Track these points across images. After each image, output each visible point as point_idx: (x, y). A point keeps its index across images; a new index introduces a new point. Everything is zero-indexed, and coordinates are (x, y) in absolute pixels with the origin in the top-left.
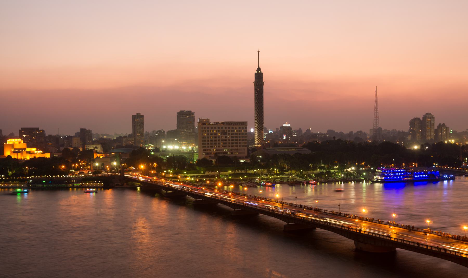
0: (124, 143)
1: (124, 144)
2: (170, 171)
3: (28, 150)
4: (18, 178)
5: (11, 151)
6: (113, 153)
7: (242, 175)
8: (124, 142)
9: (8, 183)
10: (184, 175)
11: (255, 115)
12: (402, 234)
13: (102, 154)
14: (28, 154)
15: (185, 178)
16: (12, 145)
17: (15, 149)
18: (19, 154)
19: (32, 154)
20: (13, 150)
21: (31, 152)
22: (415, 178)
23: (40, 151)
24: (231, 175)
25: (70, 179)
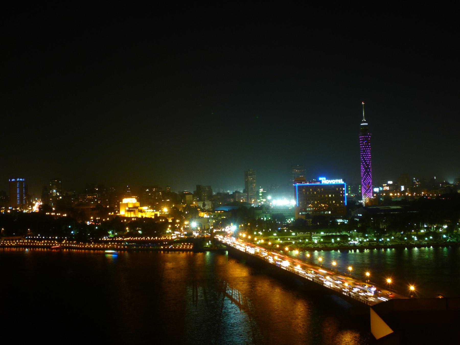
0: (237, 198)
1: (237, 200)
2: (80, 251)
3: (140, 208)
4: (82, 243)
5: (126, 210)
6: (216, 212)
7: (335, 237)
8: (236, 198)
9: (107, 245)
10: (274, 237)
11: (375, 337)
12: (375, 205)
13: (205, 213)
14: (140, 213)
15: (275, 241)
16: (127, 204)
17: (129, 208)
18: (132, 213)
19: (143, 213)
20: (127, 209)
21: (142, 211)
22: (153, 192)
23: (150, 209)
24: (323, 237)
25: (162, 241)
